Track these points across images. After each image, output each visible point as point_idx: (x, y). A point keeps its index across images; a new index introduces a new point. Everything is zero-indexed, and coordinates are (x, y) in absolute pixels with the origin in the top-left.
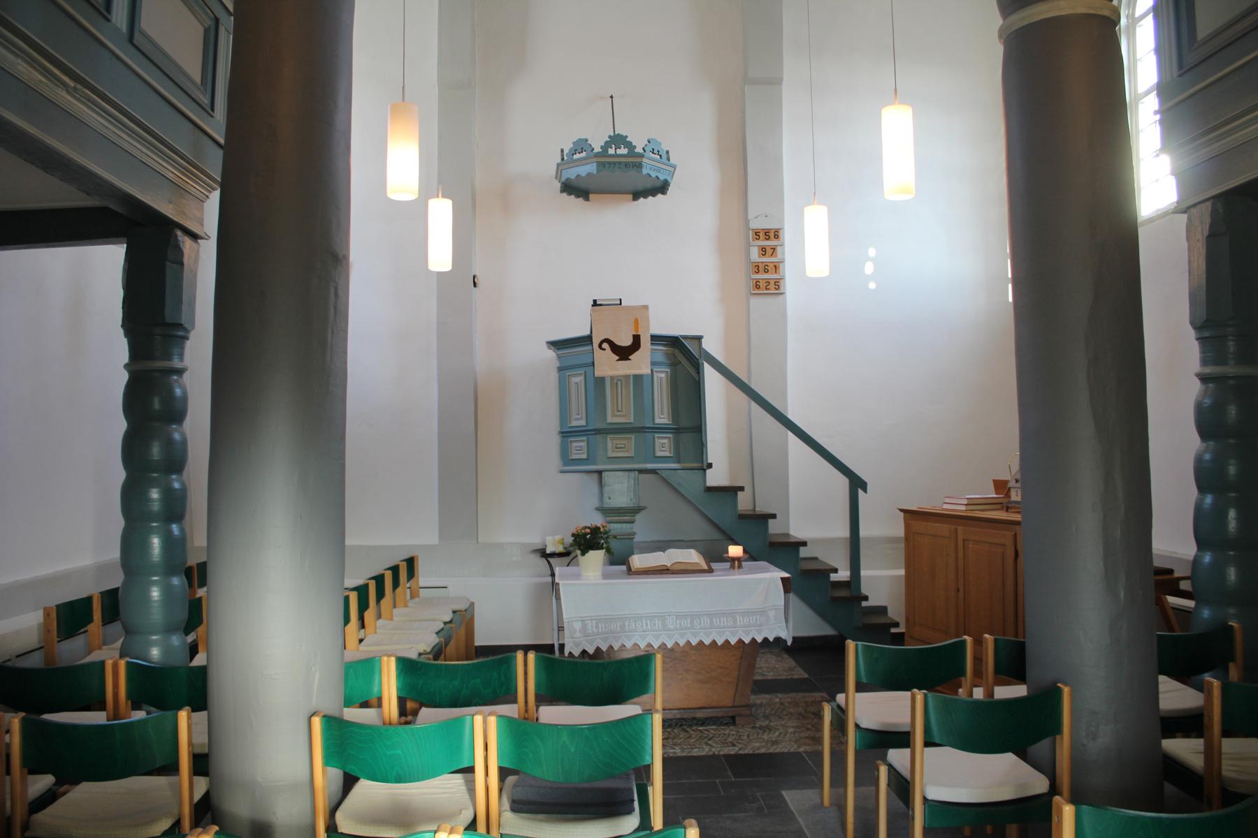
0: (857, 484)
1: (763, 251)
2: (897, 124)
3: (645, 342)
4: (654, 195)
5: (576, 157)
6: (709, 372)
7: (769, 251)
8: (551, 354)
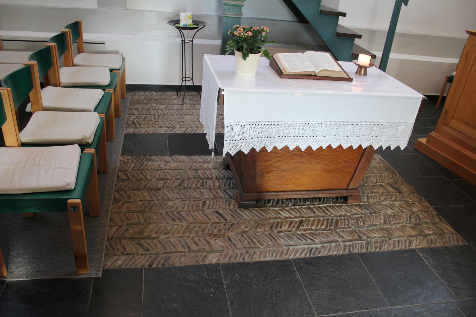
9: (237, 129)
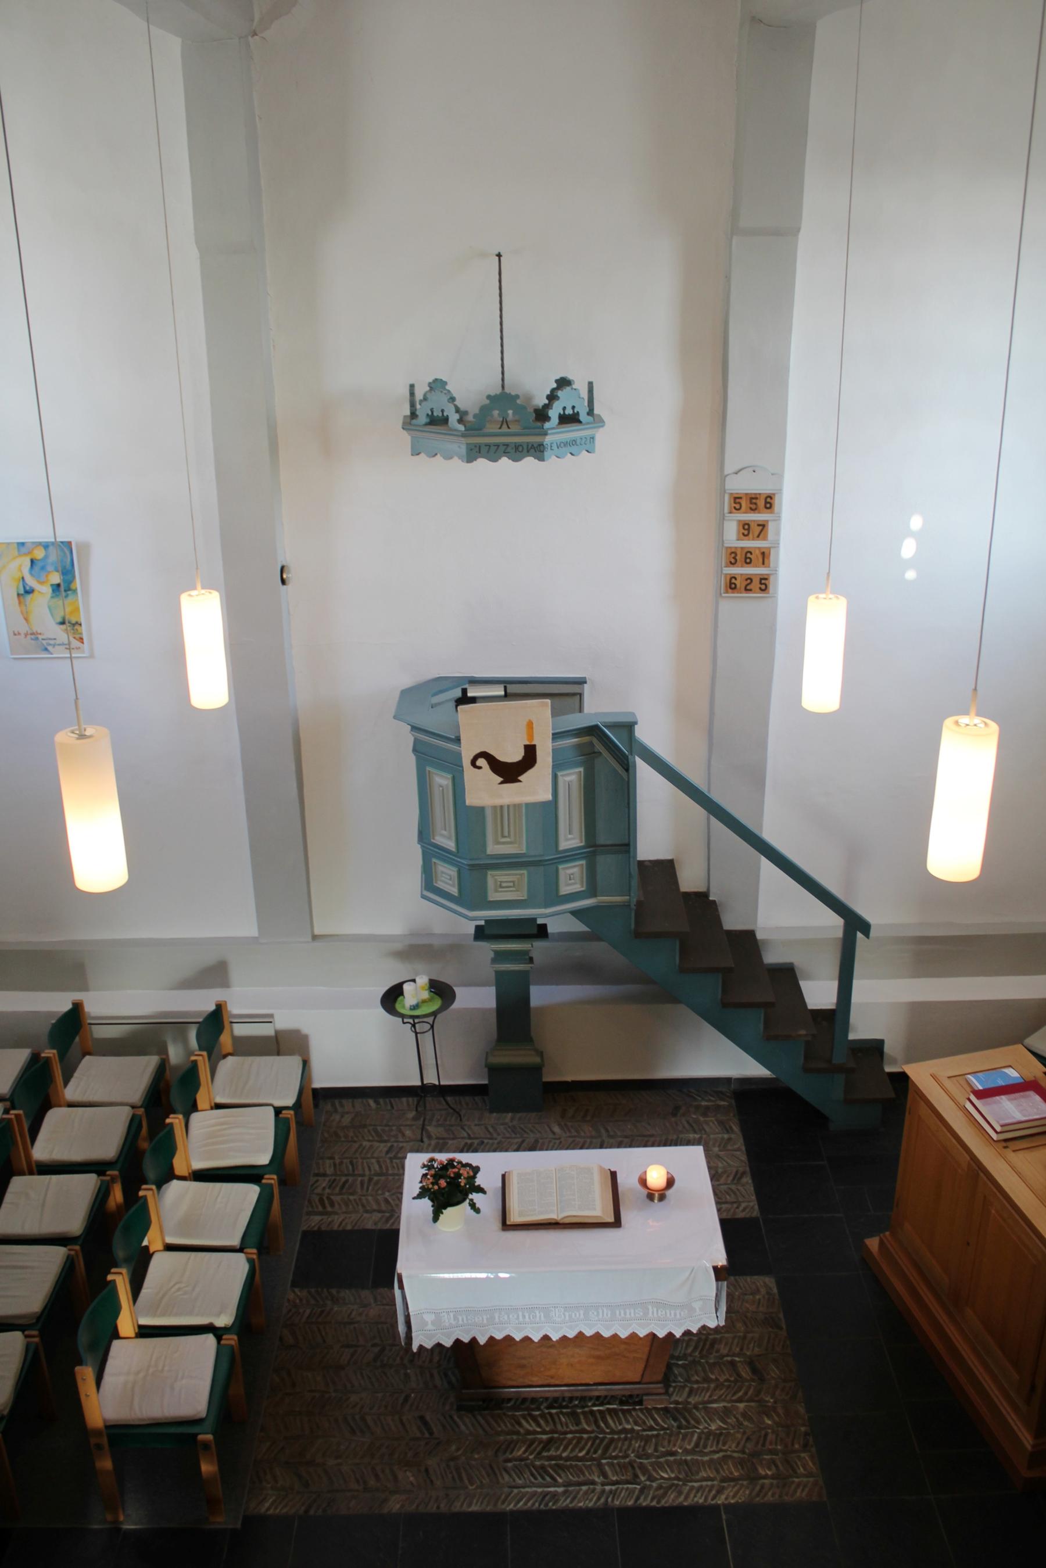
1: (746, 529)
6: (645, 773)
9: (429, 1318)
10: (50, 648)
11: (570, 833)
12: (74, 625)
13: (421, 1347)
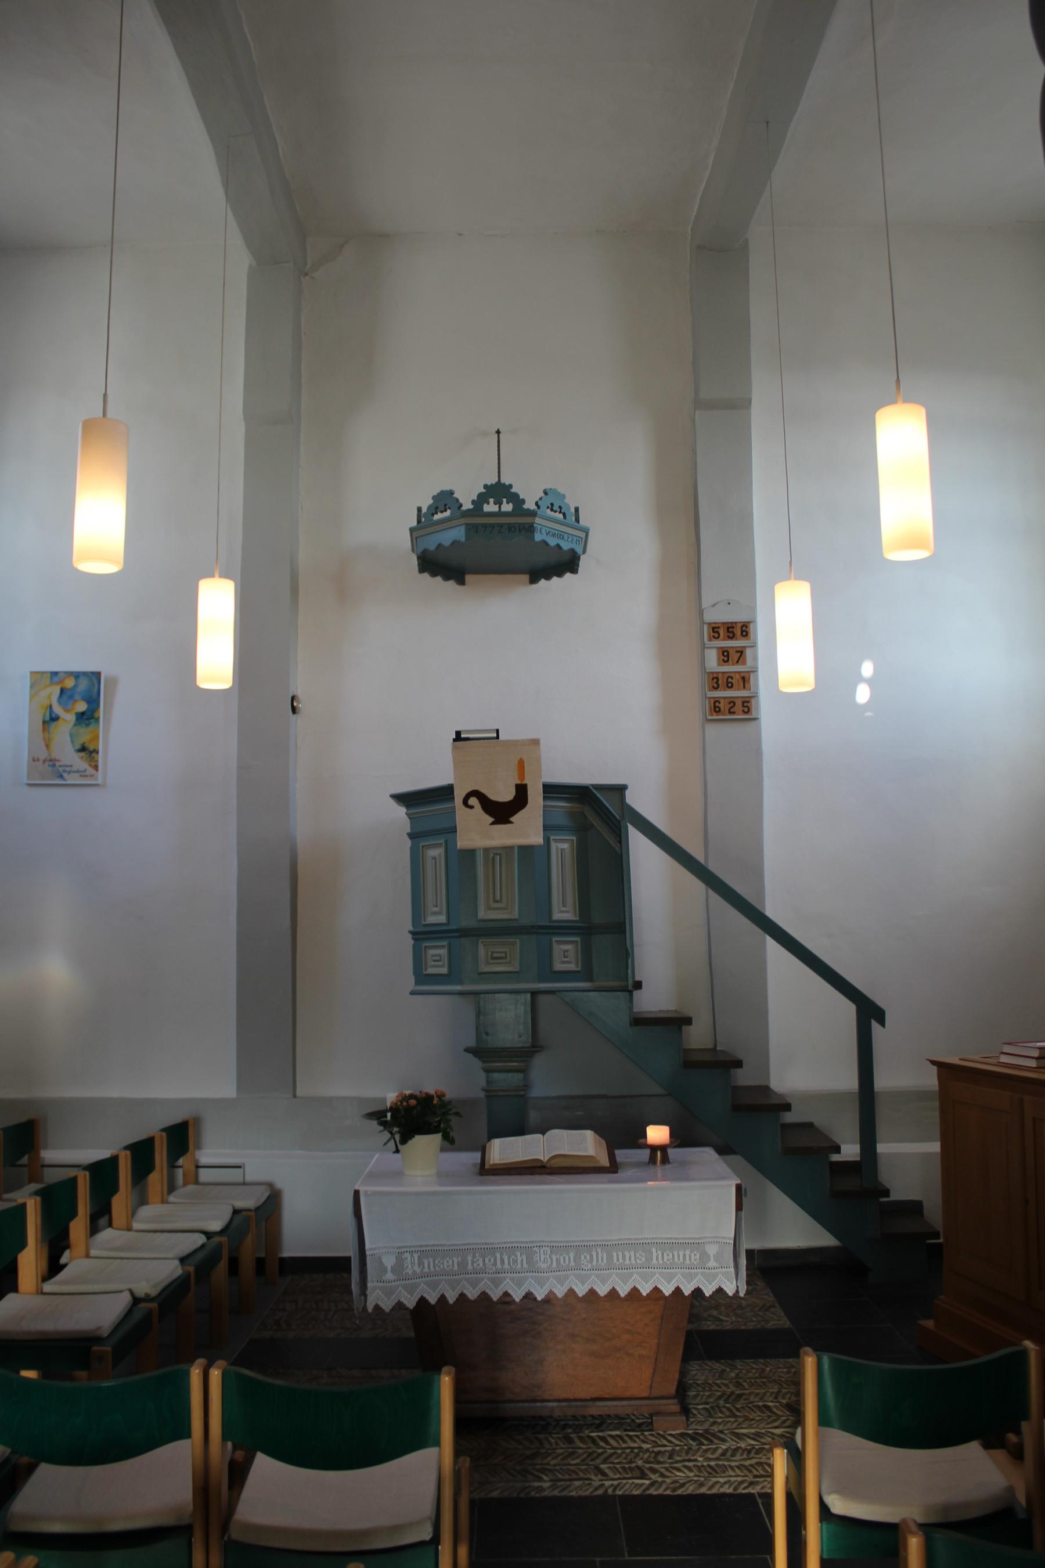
0: (869, 1013)
1: (725, 656)
2: (901, 437)
3: (536, 796)
4: (560, 575)
5: (436, 517)
6: (638, 844)
7: (734, 656)
8: (401, 811)
9: (389, 1261)
10: (65, 775)
11: (564, 905)
12: (91, 752)
13: (377, 1307)
